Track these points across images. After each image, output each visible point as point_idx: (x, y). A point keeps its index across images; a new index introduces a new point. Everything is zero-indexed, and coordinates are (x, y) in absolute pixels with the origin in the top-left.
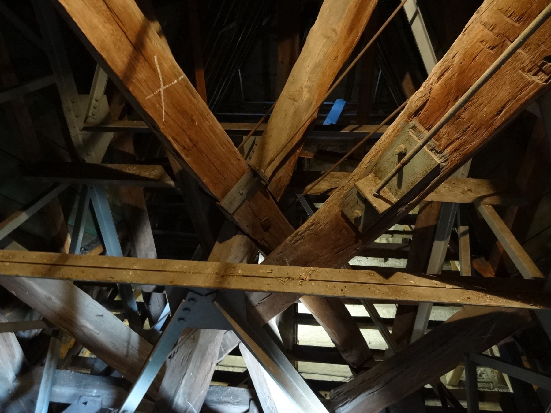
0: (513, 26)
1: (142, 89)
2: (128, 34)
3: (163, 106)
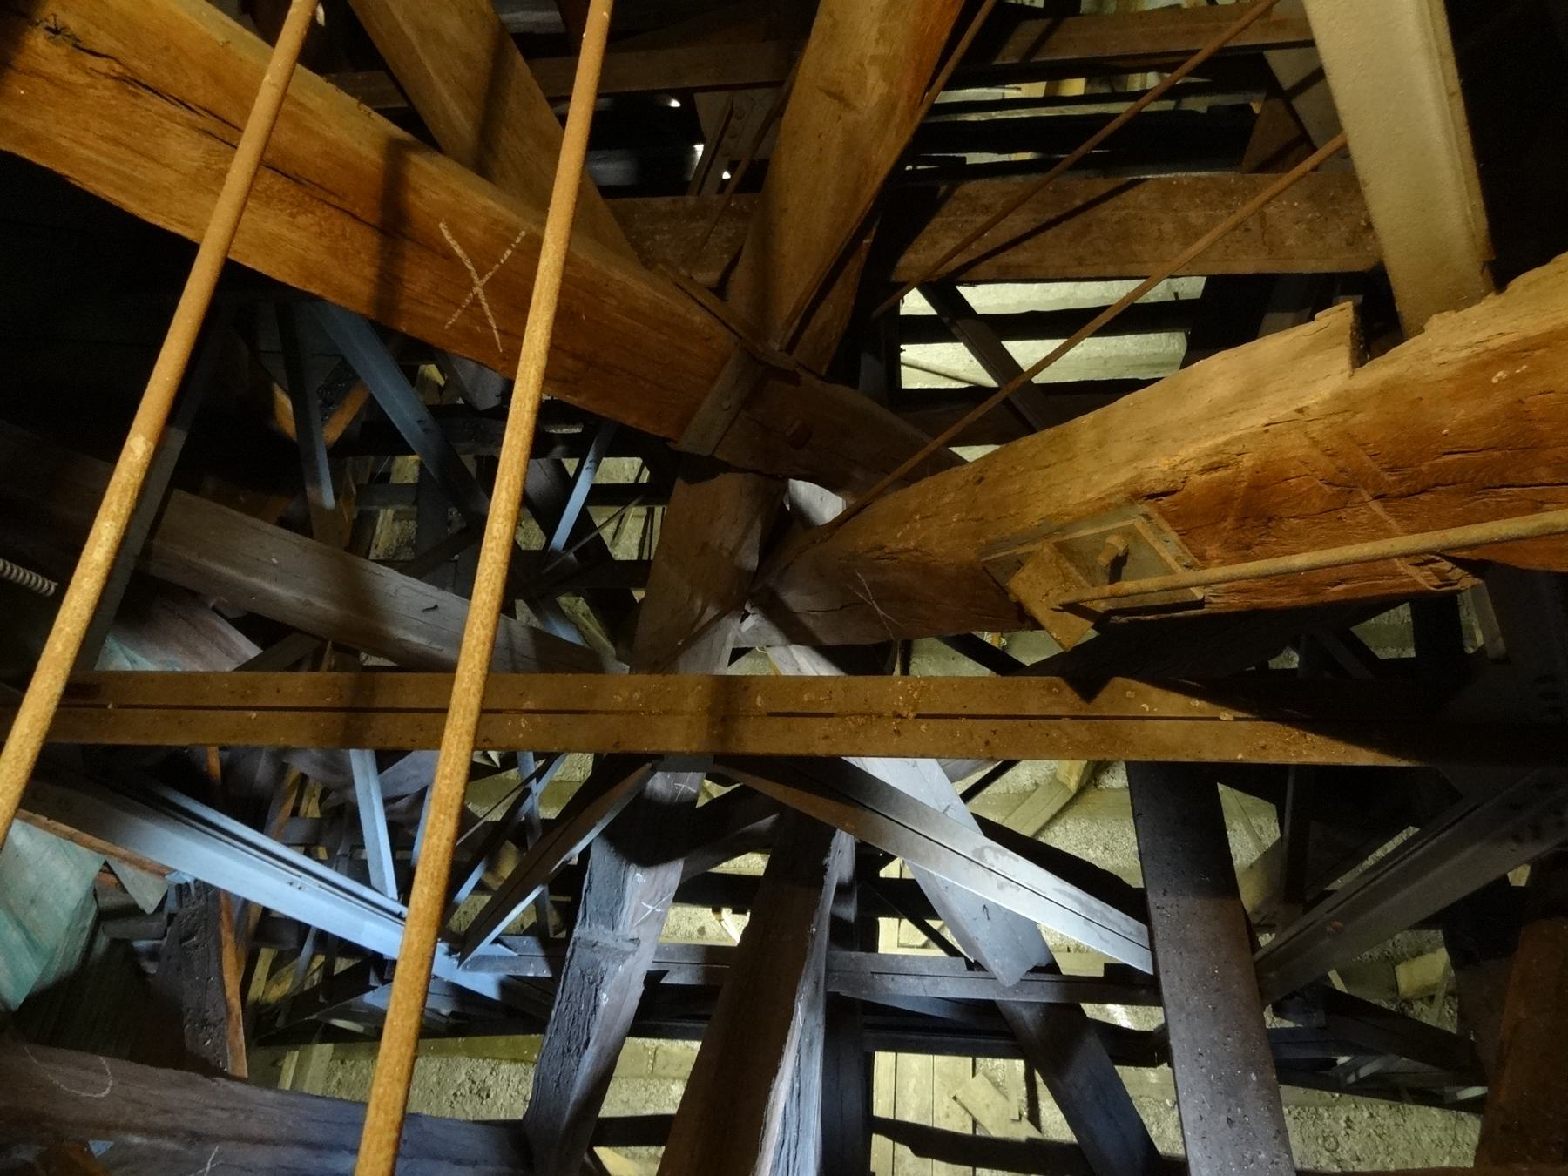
0: (1377, 475)
1: (429, 313)
2: (357, 211)
3: (492, 322)
